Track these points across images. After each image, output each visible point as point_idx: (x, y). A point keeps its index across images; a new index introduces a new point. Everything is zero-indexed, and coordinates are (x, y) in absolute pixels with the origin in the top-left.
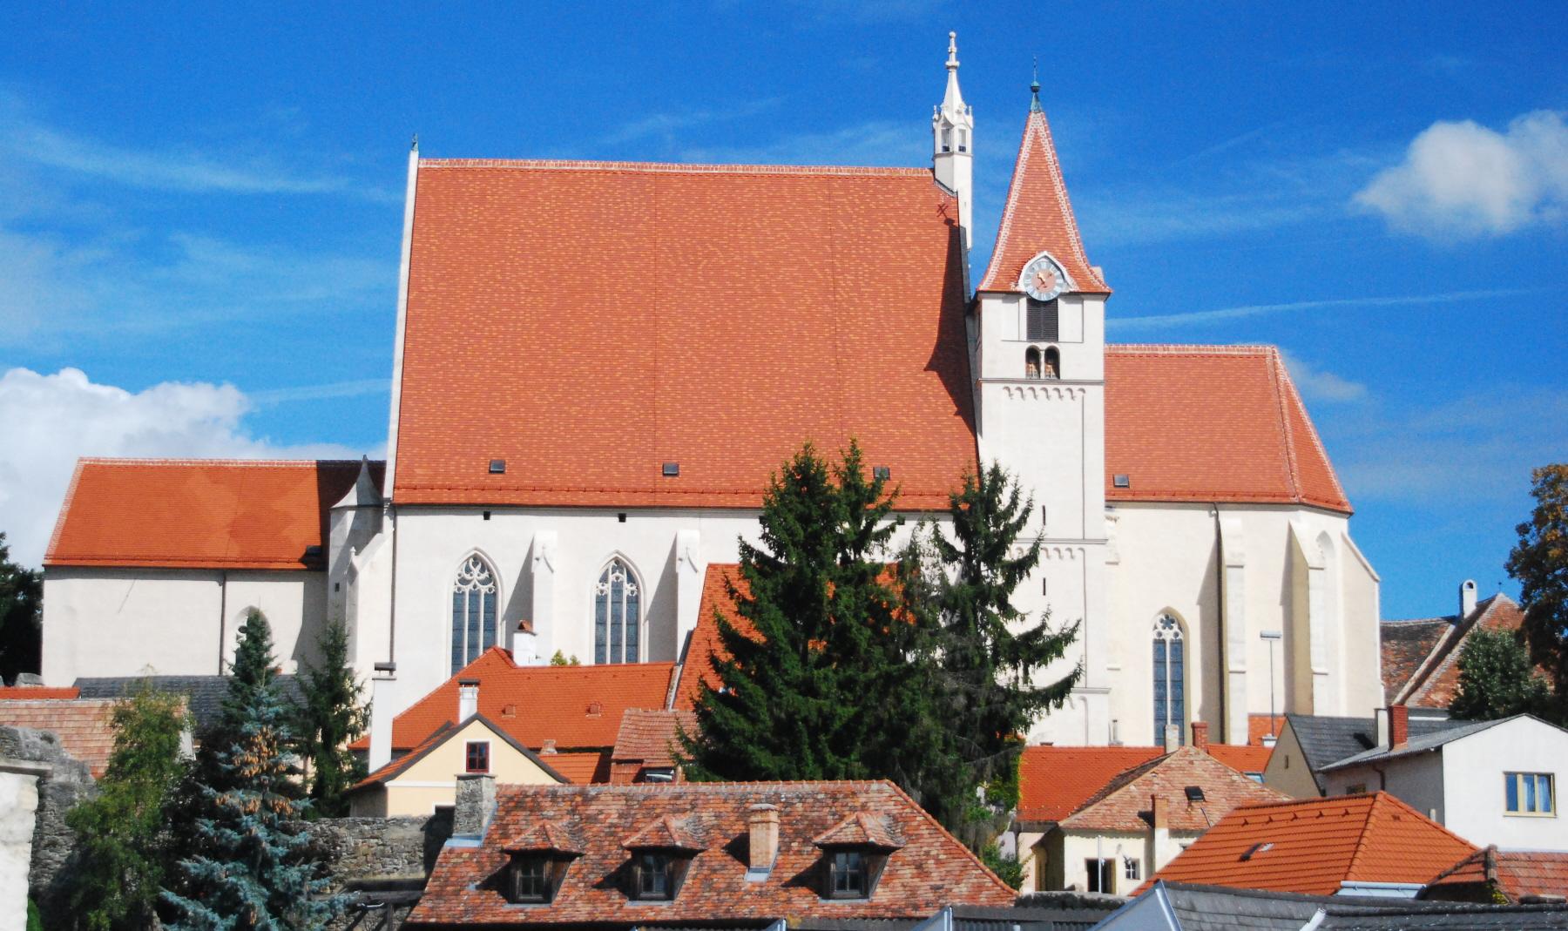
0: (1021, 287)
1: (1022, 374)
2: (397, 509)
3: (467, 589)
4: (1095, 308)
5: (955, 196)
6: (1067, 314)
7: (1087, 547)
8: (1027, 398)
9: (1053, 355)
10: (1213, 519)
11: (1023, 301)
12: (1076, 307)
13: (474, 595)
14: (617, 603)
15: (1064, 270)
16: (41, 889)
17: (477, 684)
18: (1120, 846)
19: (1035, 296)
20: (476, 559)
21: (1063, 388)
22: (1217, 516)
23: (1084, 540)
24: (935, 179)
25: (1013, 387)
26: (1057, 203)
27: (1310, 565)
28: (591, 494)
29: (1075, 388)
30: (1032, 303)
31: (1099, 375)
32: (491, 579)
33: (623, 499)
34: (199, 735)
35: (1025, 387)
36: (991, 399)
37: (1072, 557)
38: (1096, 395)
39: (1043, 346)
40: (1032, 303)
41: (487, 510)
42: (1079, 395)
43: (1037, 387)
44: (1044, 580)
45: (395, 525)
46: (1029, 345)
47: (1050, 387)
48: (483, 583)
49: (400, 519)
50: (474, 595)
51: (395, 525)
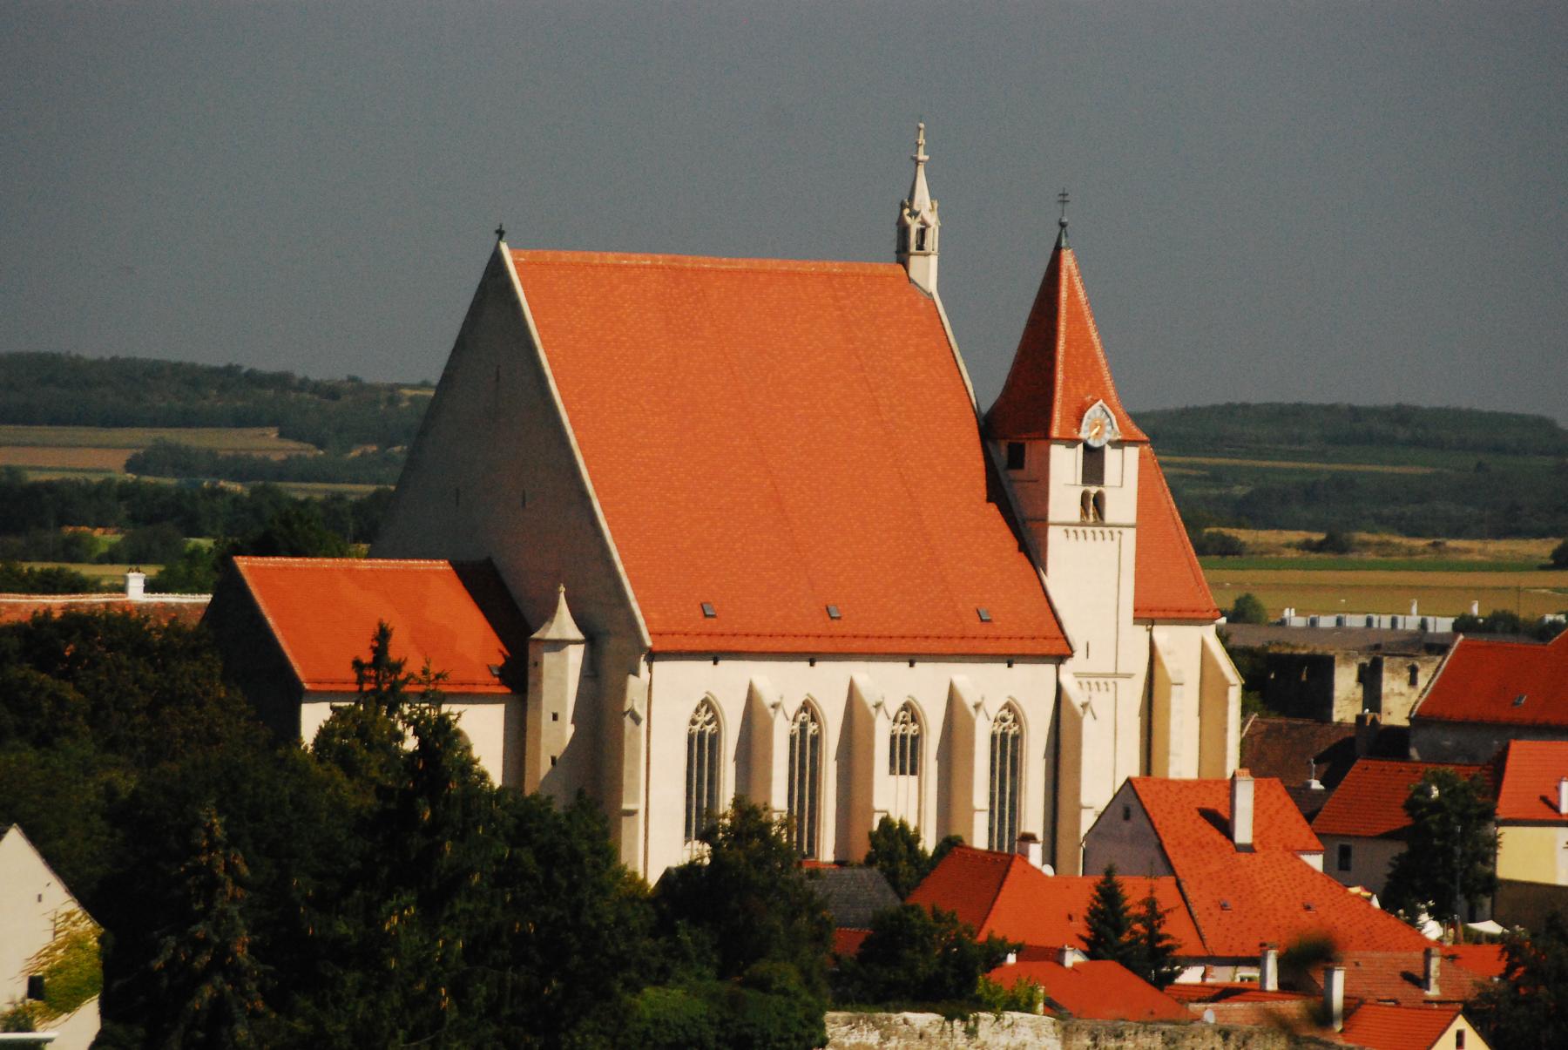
0: (1083, 435)
1: (1076, 517)
2: (652, 656)
3: (697, 728)
4: (1132, 453)
5: (931, 294)
6: (1112, 457)
7: (1118, 680)
8: (1079, 540)
9: (1099, 501)
10: (1148, 633)
11: (1080, 447)
12: (1118, 452)
13: (1004, 735)
14: (803, 741)
15: (1113, 417)
16: (215, 995)
17: (1563, 777)
18: (1230, 950)
19: (1091, 442)
20: (705, 702)
21: (1106, 530)
22: (1151, 631)
23: (1116, 675)
24: (910, 279)
25: (1071, 529)
26: (1093, 347)
27: (1174, 681)
28: (838, 640)
29: (1115, 530)
30: (1088, 449)
31: (1132, 519)
32: (715, 718)
33: (811, 645)
34: (798, 820)
35: (1079, 529)
36: (1055, 538)
37: (1107, 690)
38: (1130, 535)
39: (1093, 490)
40: (1088, 449)
41: (715, 657)
42: (1116, 536)
43: (1088, 530)
44: (1095, 718)
45: (650, 671)
46: (1083, 489)
47: (1097, 530)
48: (708, 723)
49: (657, 665)
50: (1004, 735)
51: (650, 671)
